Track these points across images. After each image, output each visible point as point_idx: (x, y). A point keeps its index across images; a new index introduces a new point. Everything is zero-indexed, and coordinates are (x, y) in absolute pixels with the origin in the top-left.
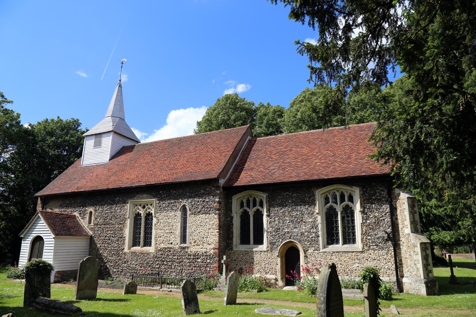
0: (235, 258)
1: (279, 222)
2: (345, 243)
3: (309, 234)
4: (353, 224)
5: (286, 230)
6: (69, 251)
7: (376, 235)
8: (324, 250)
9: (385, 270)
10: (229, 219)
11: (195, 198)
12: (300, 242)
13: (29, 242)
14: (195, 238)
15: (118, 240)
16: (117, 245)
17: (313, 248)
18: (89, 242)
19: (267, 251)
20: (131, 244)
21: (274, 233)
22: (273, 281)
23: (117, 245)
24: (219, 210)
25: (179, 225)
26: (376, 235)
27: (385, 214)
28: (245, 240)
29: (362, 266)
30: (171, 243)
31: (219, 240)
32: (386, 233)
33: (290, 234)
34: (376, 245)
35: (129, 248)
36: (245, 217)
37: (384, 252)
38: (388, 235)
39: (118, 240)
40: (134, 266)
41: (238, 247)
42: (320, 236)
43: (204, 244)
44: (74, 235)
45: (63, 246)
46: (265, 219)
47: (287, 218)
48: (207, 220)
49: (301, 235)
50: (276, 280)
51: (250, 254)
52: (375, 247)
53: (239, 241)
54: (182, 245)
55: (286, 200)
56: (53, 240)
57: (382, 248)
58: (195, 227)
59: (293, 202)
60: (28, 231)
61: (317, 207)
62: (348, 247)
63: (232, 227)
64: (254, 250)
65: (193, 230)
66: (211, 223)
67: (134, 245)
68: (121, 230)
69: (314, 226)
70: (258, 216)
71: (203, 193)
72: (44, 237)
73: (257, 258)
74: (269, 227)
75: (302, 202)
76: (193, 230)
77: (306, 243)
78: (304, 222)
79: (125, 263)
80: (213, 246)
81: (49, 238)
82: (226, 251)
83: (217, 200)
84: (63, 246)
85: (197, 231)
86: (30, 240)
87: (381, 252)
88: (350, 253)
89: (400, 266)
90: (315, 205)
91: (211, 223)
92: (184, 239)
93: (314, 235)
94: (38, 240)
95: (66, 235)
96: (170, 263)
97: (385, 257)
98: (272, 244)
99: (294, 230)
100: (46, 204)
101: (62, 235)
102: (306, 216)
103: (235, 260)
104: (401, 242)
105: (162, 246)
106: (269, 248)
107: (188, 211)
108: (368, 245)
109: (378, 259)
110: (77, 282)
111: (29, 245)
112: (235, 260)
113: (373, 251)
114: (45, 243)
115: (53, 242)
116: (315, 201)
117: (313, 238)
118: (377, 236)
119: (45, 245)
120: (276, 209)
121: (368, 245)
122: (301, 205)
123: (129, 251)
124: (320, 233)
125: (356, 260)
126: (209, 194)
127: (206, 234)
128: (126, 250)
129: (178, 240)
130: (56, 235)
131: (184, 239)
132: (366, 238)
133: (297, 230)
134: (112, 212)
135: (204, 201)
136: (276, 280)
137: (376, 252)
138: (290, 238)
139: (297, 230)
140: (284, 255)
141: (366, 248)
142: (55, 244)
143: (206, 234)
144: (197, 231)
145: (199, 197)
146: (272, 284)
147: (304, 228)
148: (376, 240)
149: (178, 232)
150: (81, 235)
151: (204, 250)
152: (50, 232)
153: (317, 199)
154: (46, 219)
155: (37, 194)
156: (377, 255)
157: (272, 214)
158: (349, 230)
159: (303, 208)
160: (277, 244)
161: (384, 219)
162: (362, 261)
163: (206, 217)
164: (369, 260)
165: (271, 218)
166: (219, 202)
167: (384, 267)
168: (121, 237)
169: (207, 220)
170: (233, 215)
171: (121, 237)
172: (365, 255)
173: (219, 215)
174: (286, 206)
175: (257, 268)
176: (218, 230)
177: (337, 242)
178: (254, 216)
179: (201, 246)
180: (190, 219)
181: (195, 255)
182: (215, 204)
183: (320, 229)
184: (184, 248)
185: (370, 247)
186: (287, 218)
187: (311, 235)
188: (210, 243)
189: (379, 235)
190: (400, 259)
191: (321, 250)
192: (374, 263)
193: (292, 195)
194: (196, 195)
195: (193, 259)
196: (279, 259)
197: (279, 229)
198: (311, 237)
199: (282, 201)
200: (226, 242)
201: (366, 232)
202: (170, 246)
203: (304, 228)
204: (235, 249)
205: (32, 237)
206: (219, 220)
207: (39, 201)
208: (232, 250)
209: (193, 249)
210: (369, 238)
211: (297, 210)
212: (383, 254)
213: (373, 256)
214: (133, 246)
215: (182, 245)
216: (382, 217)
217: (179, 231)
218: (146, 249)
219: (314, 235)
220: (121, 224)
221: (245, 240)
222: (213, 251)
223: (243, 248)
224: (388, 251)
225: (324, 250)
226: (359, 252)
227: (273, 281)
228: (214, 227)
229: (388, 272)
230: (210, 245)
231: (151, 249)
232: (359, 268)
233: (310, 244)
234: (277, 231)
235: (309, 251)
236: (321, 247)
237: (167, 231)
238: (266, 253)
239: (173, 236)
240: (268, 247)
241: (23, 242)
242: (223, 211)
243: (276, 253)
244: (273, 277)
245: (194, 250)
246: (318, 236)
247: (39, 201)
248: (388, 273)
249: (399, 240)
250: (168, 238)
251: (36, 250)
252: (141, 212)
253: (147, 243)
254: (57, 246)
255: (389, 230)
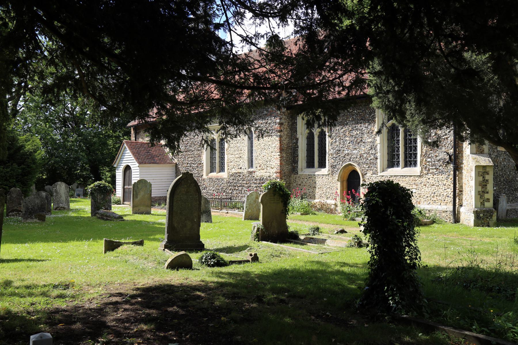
0: (300, 183)
1: (340, 143)
2: (406, 166)
3: (368, 155)
4: (416, 144)
5: (346, 152)
6: (155, 178)
7: (436, 156)
8: (382, 174)
9: (444, 198)
10: (295, 141)
11: (259, 119)
12: (359, 164)
13: (121, 171)
14: (260, 162)
15: (198, 167)
16: (197, 172)
17: (371, 172)
18: (174, 170)
19: (328, 175)
20: (209, 171)
21: (335, 155)
22: (333, 207)
23: (197, 172)
24: (280, 131)
25: (246, 149)
26: (436, 156)
27: (449, 132)
28: (310, 164)
29: (419, 192)
30: (241, 168)
31: (281, 164)
32: (448, 153)
33: (350, 156)
34: (435, 169)
35: (207, 175)
36: (310, 138)
37: (444, 176)
38: (450, 157)
39: (198, 167)
40: (212, 192)
41: (303, 170)
42: (379, 157)
43: (268, 168)
44: (158, 163)
45: (148, 173)
46: (328, 139)
47: (347, 139)
48: (270, 143)
49: (360, 157)
50: (336, 205)
51: (312, 177)
52: (435, 170)
53: (305, 164)
54: (249, 170)
55: (347, 118)
56: (138, 168)
57: (442, 173)
58: (259, 150)
59: (354, 120)
60: (120, 161)
61: (376, 126)
62: (408, 171)
63: (297, 150)
64: (316, 173)
65: (258, 153)
66: (273, 146)
67: (212, 171)
68: (200, 156)
69: (373, 147)
70: (322, 136)
71: (266, 114)
72: (131, 166)
73: (319, 182)
74: (330, 148)
75: (362, 119)
76: (258, 153)
77: (365, 166)
78: (364, 143)
79: (204, 189)
80: (275, 170)
81: (135, 166)
82: (292, 175)
83: (278, 121)
84: (148, 173)
85: (262, 155)
86: (122, 169)
87: (440, 177)
88: (408, 178)
89: (460, 193)
90: (374, 122)
91: (273, 146)
92: (251, 165)
93: (372, 157)
94: (128, 168)
95: (150, 163)
96: (240, 188)
97: (445, 182)
98: (333, 167)
99: (354, 152)
100: (138, 133)
101: (145, 163)
102: (366, 136)
103: (300, 185)
104: (463, 166)
105: (234, 171)
106: (330, 172)
107: (254, 134)
108: (427, 169)
109: (437, 184)
110: (167, 206)
111: (121, 174)
112: (300, 185)
113: (432, 176)
114: (133, 171)
115: (138, 171)
116: (375, 118)
117: (372, 161)
118: (438, 158)
119: (133, 174)
120: (337, 128)
121: (427, 169)
122: (361, 123)
123: (206, 177)
124: (378, 155)
125: (414, 185)
126: (271, 115)
127: (269, 158)
128: (205, 177)
129: (246, 165)
130: (140, 163)
131: (251, 165)
132: (426, 161)
133: (356, 152)
134: (191, 139)
135: (266, 123)
136: (336, 205)
137: (435, 176)
138: (350, 160)
139: (356, 152)
140: (346, 178)
141: (425, 172)
142: (140, 172)
143: (269, 158)
144: (262, 155)
145: (263, 119)
146: (331, 210)
147: (363, 149)
148: (436, 162)
149: (246, 156)
150: (165, 163)
151: (268, 174)
152: (135, 161)
153: (376, 116)
154: (131, 149)
155: (130, 124)
156: (436, 179)
157: (334, 135)
158: (411, 151)
159: (363, 127)
160: (337, 167)
161: (447, 138)
162: (420, 187)
163: (269, 140)
164: (427, 186)
165: (332, 139)
166: (281, 124)
167: (442, 194)
168: (200, 164)
169: (270, 143)
170: (298, 136)
171: (200, 164)
172: (423, 179)
173: (281, 137)
174: (347, 124)
175: (318, 192)
176: (279, 154)
177: (398, 165)
178: (319, 137)
179: (265, 170)
180: (255, 142)
181: (260, 180)
182: (277, 126)
183: (378, 150)
184: (251, 173)
185: (429, 170)
186: (347, 139)
187: (370, 156)
188: (273, 167)
189: (440, 157)
190: (461, 185)
191: (379, 174)
192: (432, 189)
193: (352, 112)
194: (260, 117)
195: (259, 183)
196: (339, 183)
197: (340, 151)
198: (369, 159)
199: (343, 119)
200: (292, 165)
201: (426, 153)
202: (240, 171)
203: (363, 149)
204: (299, 173)
205: (123, 167)
206: (280, 142)
207: (132, 132)
208: (297, 174)
209: (259, 174)
210: (429, 160)
211: (357, 129)
212: (443, 179)
213: (431, 181)
214: (211, 172)
215: (249, 170)
216: (446, 135)
217: (247, 156)
218: (221, 174)
219: (372, 157)
220: (199, 150)
221: (310, 164)
222: (275, 175)
223: (308, 171)
224: (449, 175)
225: (382, 174)
226: (417, 176)
227: (333, 207)
228: (276, 149)
229: (446, 200)
230: (273, 168)
231: (224, 175)
232: (416, 195)
233: (369, 167)
234: (338, 153)
235: (368, 175)
236: (379, 170)
237: (237, 156)
238: (327, 177)
239: (242, 160)
240: (329, 170)
241: (117, 171)
242: (286, 133)
243: (336, 177)
244: (333, 202)
245: (260, 175)
246: (377, 159)
247: (132, 132)
248: (446, 201)
249: (462, 163)
250: (238, 163)
251: (127, 178)
252: (215, 137)
253: (222, 169)
254: (142, 174)
255: (451, 151)
